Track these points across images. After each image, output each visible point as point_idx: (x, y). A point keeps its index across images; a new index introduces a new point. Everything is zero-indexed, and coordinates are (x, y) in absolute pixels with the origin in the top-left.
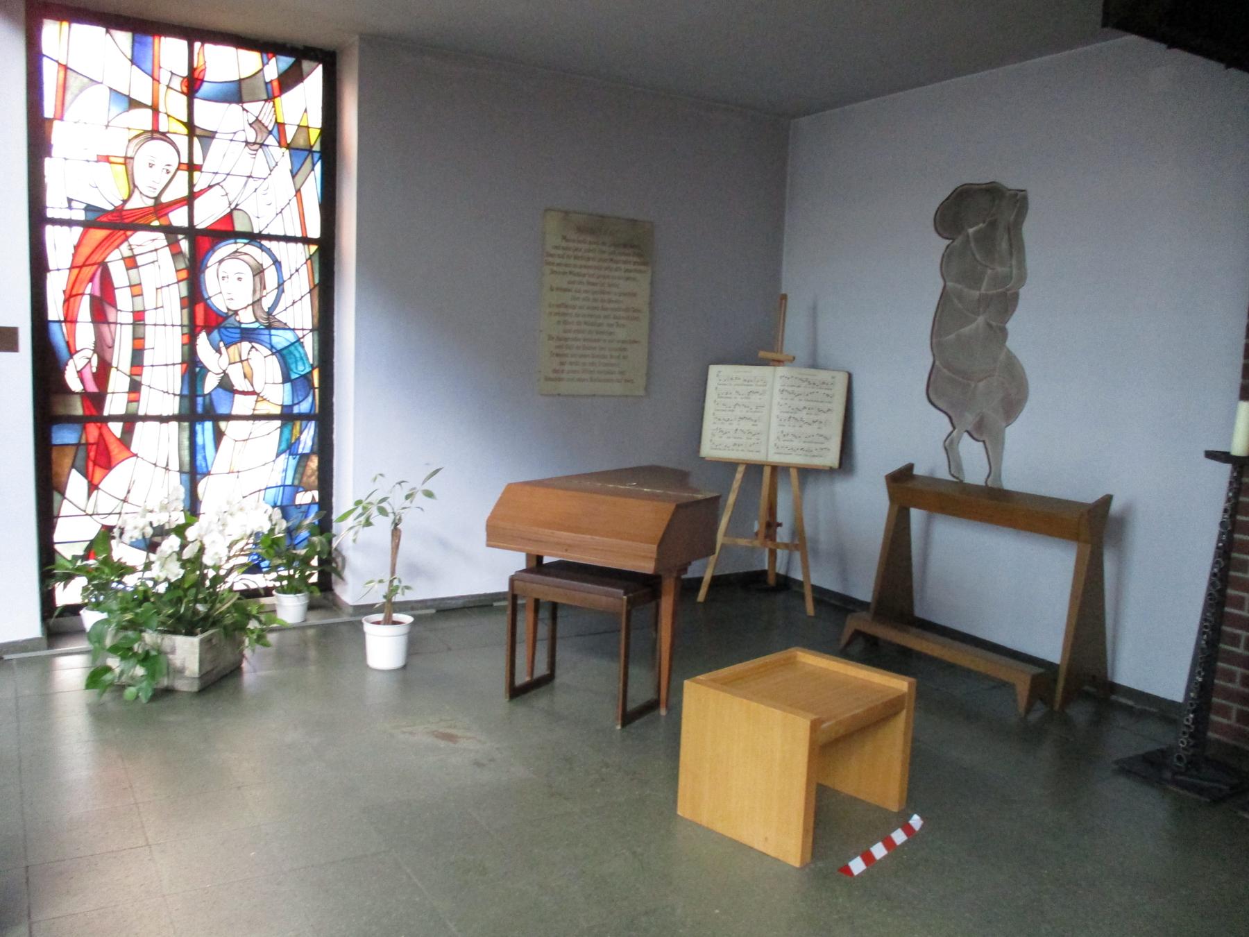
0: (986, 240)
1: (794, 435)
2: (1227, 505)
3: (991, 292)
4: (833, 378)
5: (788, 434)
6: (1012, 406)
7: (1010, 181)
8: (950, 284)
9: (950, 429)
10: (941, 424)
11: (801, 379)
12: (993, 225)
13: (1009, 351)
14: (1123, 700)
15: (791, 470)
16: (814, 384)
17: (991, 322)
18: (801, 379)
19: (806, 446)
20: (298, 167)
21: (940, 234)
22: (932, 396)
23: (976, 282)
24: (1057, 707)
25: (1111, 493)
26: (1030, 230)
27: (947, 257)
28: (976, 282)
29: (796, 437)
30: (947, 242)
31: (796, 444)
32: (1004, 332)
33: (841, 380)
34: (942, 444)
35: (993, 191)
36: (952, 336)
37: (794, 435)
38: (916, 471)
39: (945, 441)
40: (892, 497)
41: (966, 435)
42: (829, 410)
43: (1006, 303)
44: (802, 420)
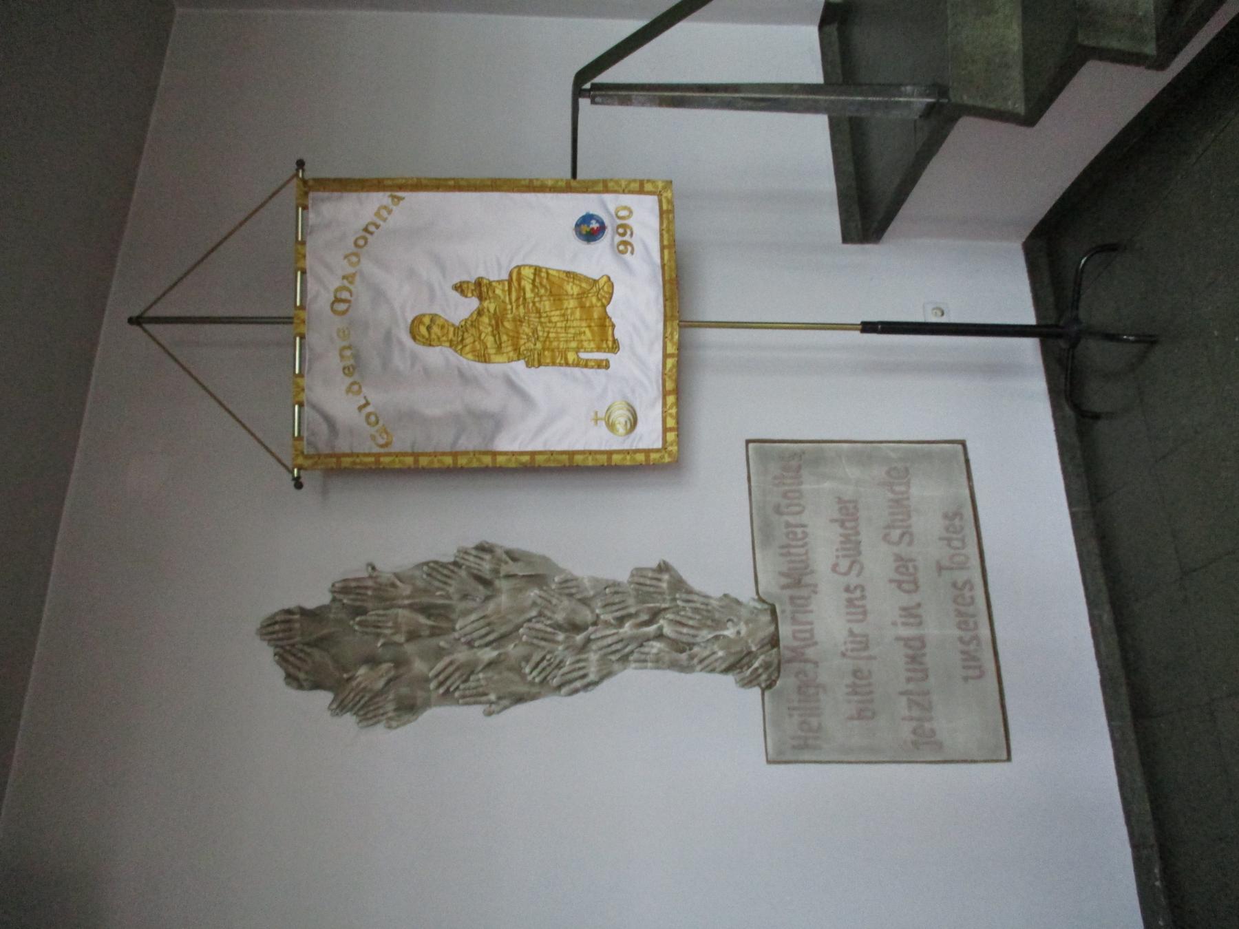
2: (587, 583)
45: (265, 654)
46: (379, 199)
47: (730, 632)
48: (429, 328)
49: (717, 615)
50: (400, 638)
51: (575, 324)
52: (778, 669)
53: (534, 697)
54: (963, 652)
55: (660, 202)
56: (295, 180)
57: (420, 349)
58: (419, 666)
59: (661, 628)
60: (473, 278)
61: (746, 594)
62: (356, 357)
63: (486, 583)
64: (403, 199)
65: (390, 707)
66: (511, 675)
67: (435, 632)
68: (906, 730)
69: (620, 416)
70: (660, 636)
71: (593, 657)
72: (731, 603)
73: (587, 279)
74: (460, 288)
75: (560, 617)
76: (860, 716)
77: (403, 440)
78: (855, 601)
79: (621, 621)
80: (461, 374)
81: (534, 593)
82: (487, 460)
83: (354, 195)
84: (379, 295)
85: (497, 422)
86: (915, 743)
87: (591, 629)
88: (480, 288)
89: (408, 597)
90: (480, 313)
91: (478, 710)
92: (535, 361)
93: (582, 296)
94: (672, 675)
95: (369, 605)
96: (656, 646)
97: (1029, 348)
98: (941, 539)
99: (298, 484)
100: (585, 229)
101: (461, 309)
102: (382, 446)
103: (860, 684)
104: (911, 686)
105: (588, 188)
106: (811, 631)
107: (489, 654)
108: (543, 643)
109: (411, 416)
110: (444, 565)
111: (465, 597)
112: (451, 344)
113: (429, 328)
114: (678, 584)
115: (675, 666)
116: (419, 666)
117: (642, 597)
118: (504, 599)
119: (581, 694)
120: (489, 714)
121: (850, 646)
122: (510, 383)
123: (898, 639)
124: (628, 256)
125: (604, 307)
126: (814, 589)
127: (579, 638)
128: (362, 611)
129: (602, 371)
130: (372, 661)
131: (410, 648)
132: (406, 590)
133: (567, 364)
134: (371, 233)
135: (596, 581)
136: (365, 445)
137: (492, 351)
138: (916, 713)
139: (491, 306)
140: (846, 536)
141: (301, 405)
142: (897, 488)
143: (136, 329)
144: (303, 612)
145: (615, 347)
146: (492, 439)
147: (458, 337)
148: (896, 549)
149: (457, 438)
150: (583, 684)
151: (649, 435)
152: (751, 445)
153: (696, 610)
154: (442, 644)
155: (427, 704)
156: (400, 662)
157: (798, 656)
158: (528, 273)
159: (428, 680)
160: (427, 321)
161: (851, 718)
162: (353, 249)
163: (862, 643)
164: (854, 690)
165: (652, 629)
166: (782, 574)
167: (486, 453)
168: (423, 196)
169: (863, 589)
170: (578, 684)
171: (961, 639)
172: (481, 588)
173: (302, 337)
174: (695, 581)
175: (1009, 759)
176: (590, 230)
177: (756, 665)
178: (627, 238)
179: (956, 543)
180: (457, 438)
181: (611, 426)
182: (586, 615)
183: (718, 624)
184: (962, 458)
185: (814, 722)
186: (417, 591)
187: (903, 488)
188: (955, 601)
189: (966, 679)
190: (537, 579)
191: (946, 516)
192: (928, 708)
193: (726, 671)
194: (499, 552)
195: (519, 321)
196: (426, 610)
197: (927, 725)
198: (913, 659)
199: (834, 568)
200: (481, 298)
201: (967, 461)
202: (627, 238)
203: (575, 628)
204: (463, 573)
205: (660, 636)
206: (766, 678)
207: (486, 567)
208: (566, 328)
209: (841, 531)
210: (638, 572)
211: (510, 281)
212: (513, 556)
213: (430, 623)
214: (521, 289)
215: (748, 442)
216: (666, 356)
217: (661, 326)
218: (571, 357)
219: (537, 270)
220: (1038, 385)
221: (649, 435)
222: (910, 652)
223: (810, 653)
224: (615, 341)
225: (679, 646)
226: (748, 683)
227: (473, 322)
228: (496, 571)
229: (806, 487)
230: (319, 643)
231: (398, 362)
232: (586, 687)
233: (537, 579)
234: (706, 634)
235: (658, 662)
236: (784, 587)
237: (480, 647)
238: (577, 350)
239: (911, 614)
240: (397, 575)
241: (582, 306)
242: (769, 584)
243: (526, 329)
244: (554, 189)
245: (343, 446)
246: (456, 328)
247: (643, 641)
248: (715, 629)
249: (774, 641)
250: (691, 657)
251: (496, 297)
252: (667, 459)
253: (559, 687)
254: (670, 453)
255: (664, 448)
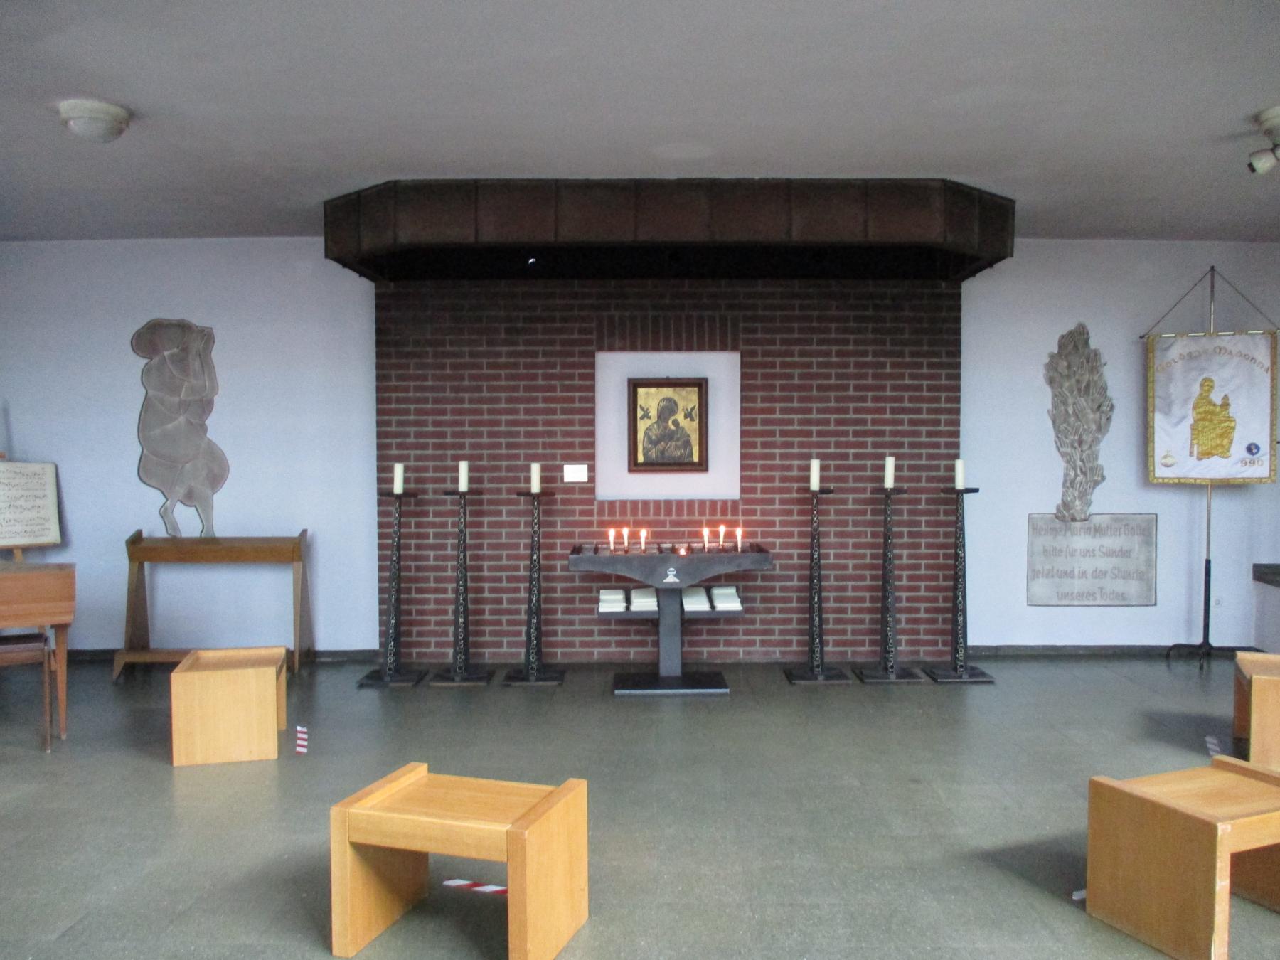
0: (181, 360)
1: (15, 520)
2: (1097, 448)
3: (191, 398)
4: (43, 469)
5: (10, 521)
6: (217, 477)
7: (197, 320)
8: (151, 393)
9: (165, 500)
10: (154, 498)
11: (15, 472)
12: (185, 350)
13: (209, 440)
14: (323, 660)
15: (15, 551)
16: (27, 475)
17: (191, 420)
18: (15, 472)
19: (28, 529)
20: (1098, 516)
21: (134, 350)
22: (141, 474)
23: (175, 390)
24: (296, 670)
25: (305, 528)
26: (217, 355)
27: (146, 372)
28: (175, 390)
29: (19, 522)
30: (146, 361)
31: (18, 528)
32: (204, 428)
33: (50, 470)
34: (158, 513)
35: (183, 327)
36: (157, 431)
37: (15, 520)
38: (145, 535)
39: (161, 509)
40: (132, 557)
41: (179, 503)
42: (44, 496)
43: (206, 406)
44: (21, 506)
45: (1071, 326)
46: (1267, 363)
47: (1077, 503)
48: (1208, 385)
49: (1084, 498)
50: (1077, 377)
51: (1210, 443)
52: (1062, 521)
53: (1054, 427)
54: (1068, 593)
55: (1265, 478)
56: (1275, 329)
57: (1200, 380)
58: (1067, 384)
59: (1079, 476)
60: (1230, 402)
61: (1093, 509)
62: (1196, 357)
63: (1099, 407)
64: (1267, 372)
65: (1051, 374)
66: (1062, 418)
67: (1079, 390)
68: (1039, 567)
69: (1169, 461)
70: (1076, 475)
71: (1069, 450)
72: (1089, 504)
73: (1229, 447)
74: (1226, 397)
75: (1084, 437)
76: (1045, 551)
77: (1160, 377)
78: (1088, 553)
79: (1082, 460)
80: (1189, 398)
81: (1094, 427)
82: (1151, 409)
83: (1269, 353)
84: (1223, 365)
85: (1167, 412)
86: (1034, 570)
87: (1080, 449)
88: (1226, 405)
89: (1093, 380)
90: (1215, 405)
91: (1050, 407)
92: (1193, 427)
93: (1222, 446)
94: (1061, 480)
95: (1090, 364)
96: (1072, 474)
97: (1197, 640)
98: (1113, 590)
99: (1141, 337)
100: (1253, 447)
101: (1216, 397)
102: (1157, 368)
103: (1056, 552)
104: (1055, 571)
105: (1272, 448)
106: (1077, 534)
107: (1070, 411)
108: (1074, 431)
109: (1170, 379)
110: (1105, 392)
111: (1093, 400)
112: (1201, 394)
113: (1208, 385)
114: (1096, 483)
115: (1065, 481)
116: (1067, 384)
117: (1091, 469)
118: (1091, 416)
119: (1055, 446)
120: (1048, 411)
121: (1071, 550)
122: (1184, 417)
123: (1074, 568)
124: (1240, 464)
125: (1217, 455)
126: (1094, 537)
127: (1076, 445)
128: (1088, 362)
129: (1189, 454)
130: (1069, 367)
131: (1073, 381)
132: (1096, 378)
133: (1192, 440)
134: (1251, 360)
135: (1098, 451)
136: (1158, 362)
137: (1198, 410)
138: (1046, 572)
139: (1218, 409)
140: (1115, 552)
141: (1175, 337)
142: (1135, 575)
143: (1209, 268)
144: (1088, 339)
145: (1199, 459)
146: (1160, 410)
147: (1204, 398)
148: (1109, 572)
149: (1159, 397)
150: (1059, 444)
151: (1160, 472)
152: (1154, 516)
153: (1086, 490)
154: (1075, 393)
155: (1052, 388)
156: (1068, 377)
157: (1068, 529)
158: (1233, 424)
159: (1061, 388)
160: (1211, 384)
161: (1044, 547)
162: (1243, 353)
163: (1072, 554)
164: (1054, 549)
165: (1079, 472)
166: (1100, 525)
167: (1154, 409)
168: (1268, 380)
169: (1094, 556)
170: (1059, 444)
171: (1072, 594)
172: (1096, 407)
173: (1204, 336)
174: (1098, 490)
175: (1028, 605)
176: (1252, 449)
177: (1064, 512)
178: (1248, 464)
179: (1112, 596)
180: (1159, 397)
181: (1165, 457)
182: (1085, 447)
183: (1081, 498)
184: (1148, 604)
185: (1043, 533)
186: (1095, 382)
187: (1135, 578)
188: (1088, 593)
189: (1058, 593)
190: (1099, 429)
191: (1123, 594)
192: (1047, 576)
193: (1062, 500)
194: (1111, 413)
195: (1211, 421)
196: (1088, 386)
197: (1041, 575)
198: (1066, 573)
199: (1102, 546)
200: (1221, 406)
201: (1147, 606)
202: (1248, 464)
203: (1081, 442)
204: (1102, 400)
205: (1076, 475)
206: (1059, 516)
207: (1104, 408)
208: (1208, 439)
209: (1117, 550)
210: (1102, 468)
211: (1229, 417)
212: (1109, 419)
213: (1082, 388)
214: (1225, 421)
215: (1156, 515)
216: (1195, 479)
217: (1208, 477)
218: (1195, 442)
219: (1234, 428)
220: (1182, 640)
221: (1160, 472)
222: (1068, 572)
223: (1069, 534)
224: (1201, 459)
225: (1072, 482)
226: (1058, 509)
227: (1210, 403)
228: (1103, 412)
229: (1136, 537)
230: (1076, 347)
231: (1194, 373)
232: (1057, 447)
233: (1099, 429)
234: (1076, 493)
235: (1066, 475)
236: (1095, 525)
237: (1073, 407)
238: (1198, 444)
239: (1083, 574)
240: (1102, 374)
241: (1217, 446)
242: (1096, 520)
243: (1207, 424)
244: (1272, 435)
245: (1158, 353)
246: (1208, 396)
247: (1075, 469)
248: (1079, 497)
249: (1074, 519)
250: (1068, 487)
251: (1222, 411)
252: (1151, 479)
253: (1058, 437)
254: (1153, 480)
255: (1155, 478)
